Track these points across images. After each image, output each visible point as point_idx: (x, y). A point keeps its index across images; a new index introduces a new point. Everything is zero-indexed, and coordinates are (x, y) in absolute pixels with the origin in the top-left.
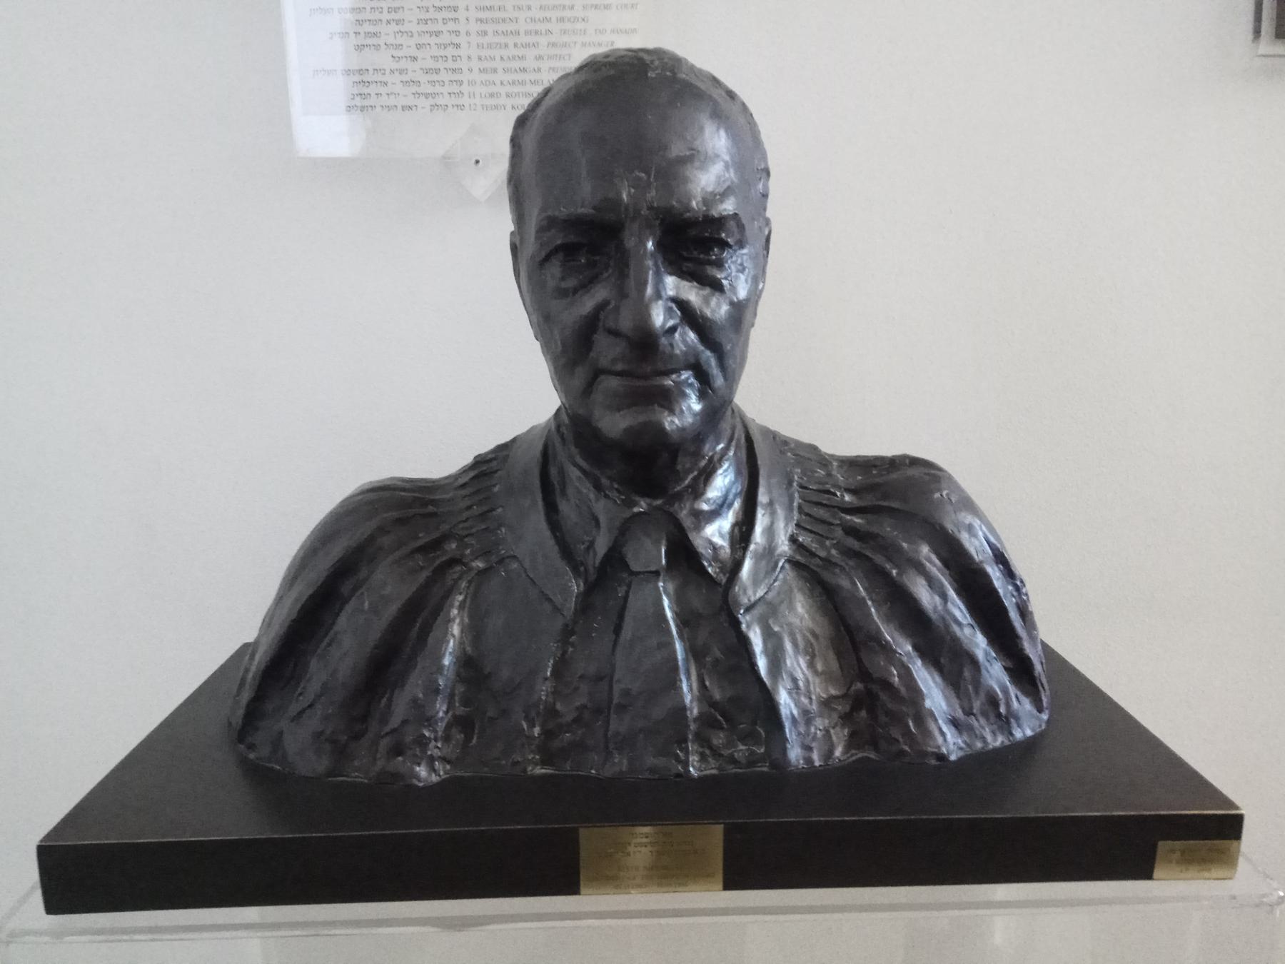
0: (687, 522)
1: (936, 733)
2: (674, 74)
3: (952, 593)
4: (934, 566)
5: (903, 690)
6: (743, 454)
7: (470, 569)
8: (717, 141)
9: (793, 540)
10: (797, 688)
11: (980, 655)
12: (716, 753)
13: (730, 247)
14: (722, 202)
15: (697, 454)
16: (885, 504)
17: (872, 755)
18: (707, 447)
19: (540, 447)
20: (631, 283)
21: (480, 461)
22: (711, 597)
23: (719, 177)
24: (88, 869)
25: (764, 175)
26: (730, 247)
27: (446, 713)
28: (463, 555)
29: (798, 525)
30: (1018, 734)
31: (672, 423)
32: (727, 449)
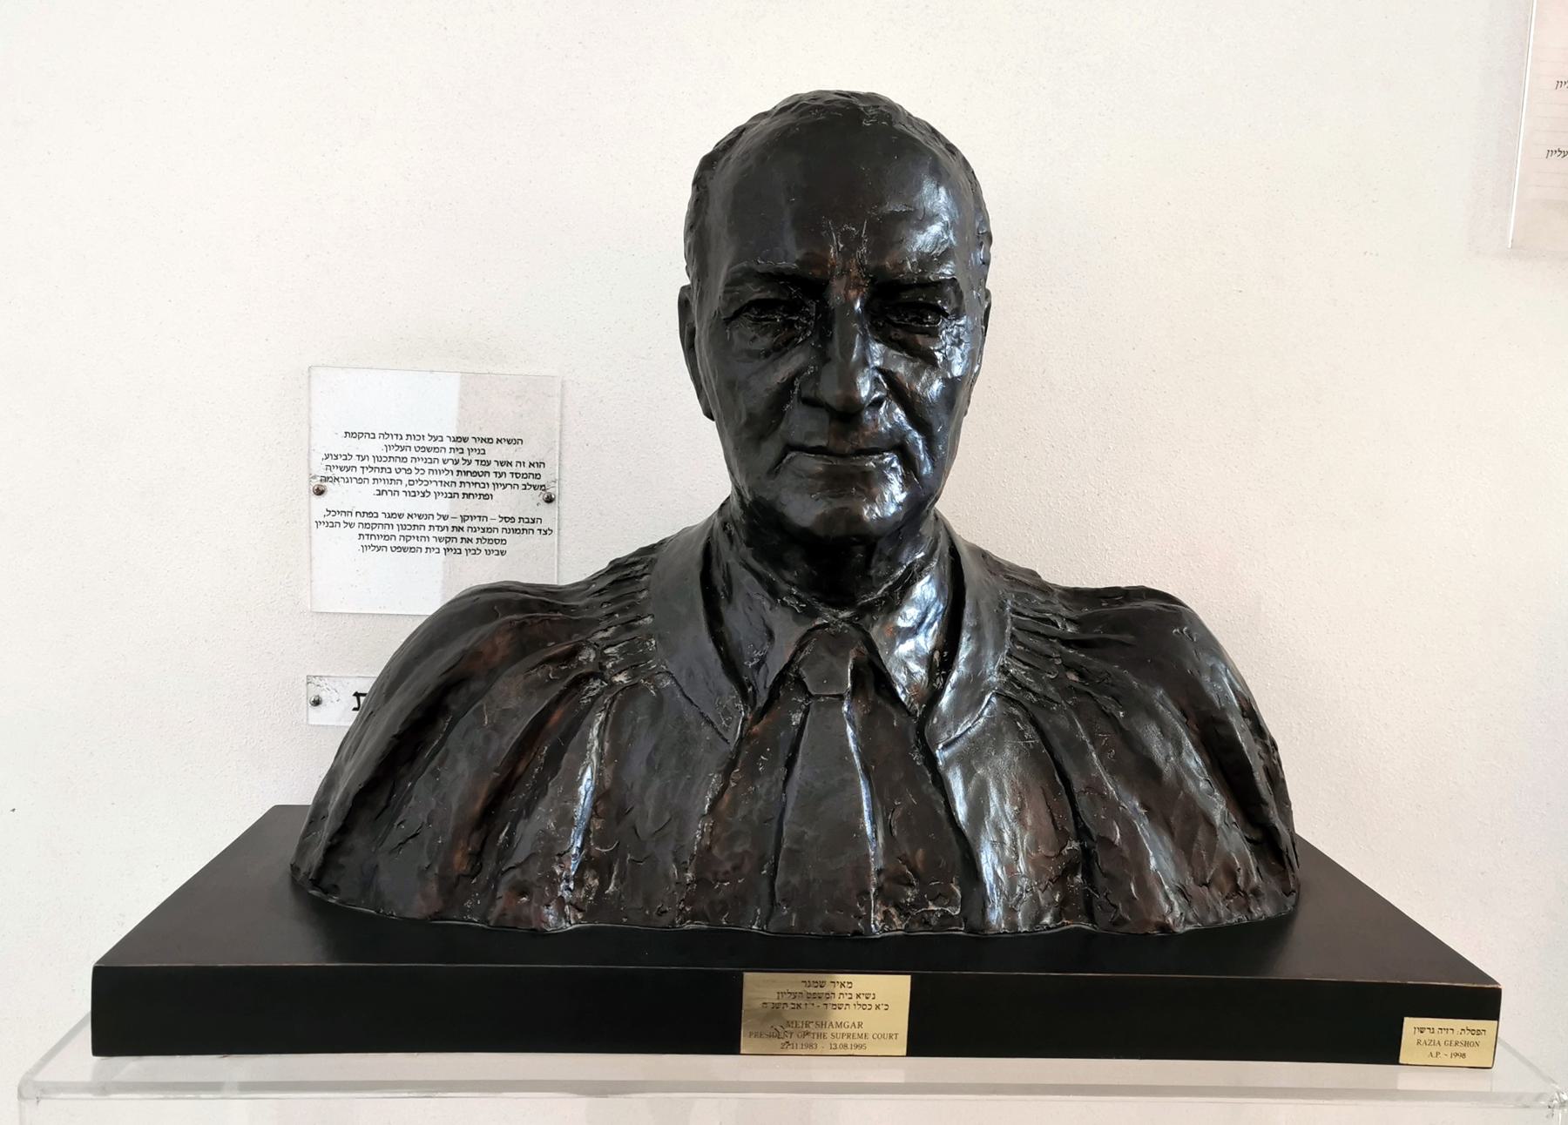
0: (880, 643)
1: (1161, 898)
2: (891, 123)
3: (1187, 743)
4: (1171, 713)
5: (1127, 853)
6: (947, 568)
7: (612, 685)
8: (938, 199)
9: (1003, 670)
10: (1002, 843)
11: (1218, 820)
12: (903, 910)
13: (946, 315)
14: (939, 265)
15: (894, 562)
16: (1113, 637)
17: (1088, 927)
18: (905, 555)
19: (702, 542)
20: (835, 347)
21: (616, 566)
22: (903, 738)
23: (937, 237)
24: (150, 1003)
25: (985, 240)
26: (946, 315)
27: (581, 849)
28: (602, 668)
29: (1010, 655)
30: (1257, 913)
31: (871, 513)
32: (928, 558)
